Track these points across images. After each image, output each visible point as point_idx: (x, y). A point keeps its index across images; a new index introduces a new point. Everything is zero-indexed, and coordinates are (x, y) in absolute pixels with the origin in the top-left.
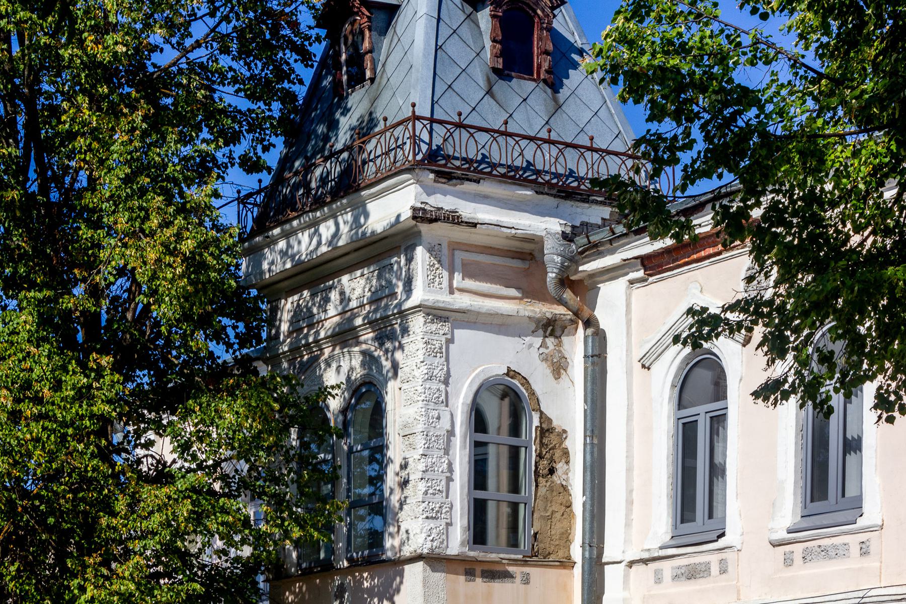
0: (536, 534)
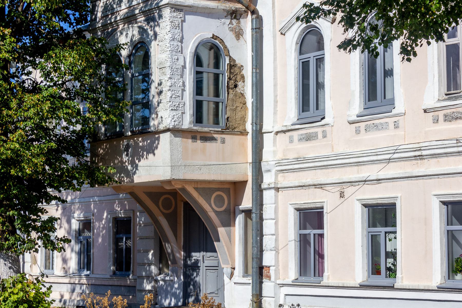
0: (228, 118)
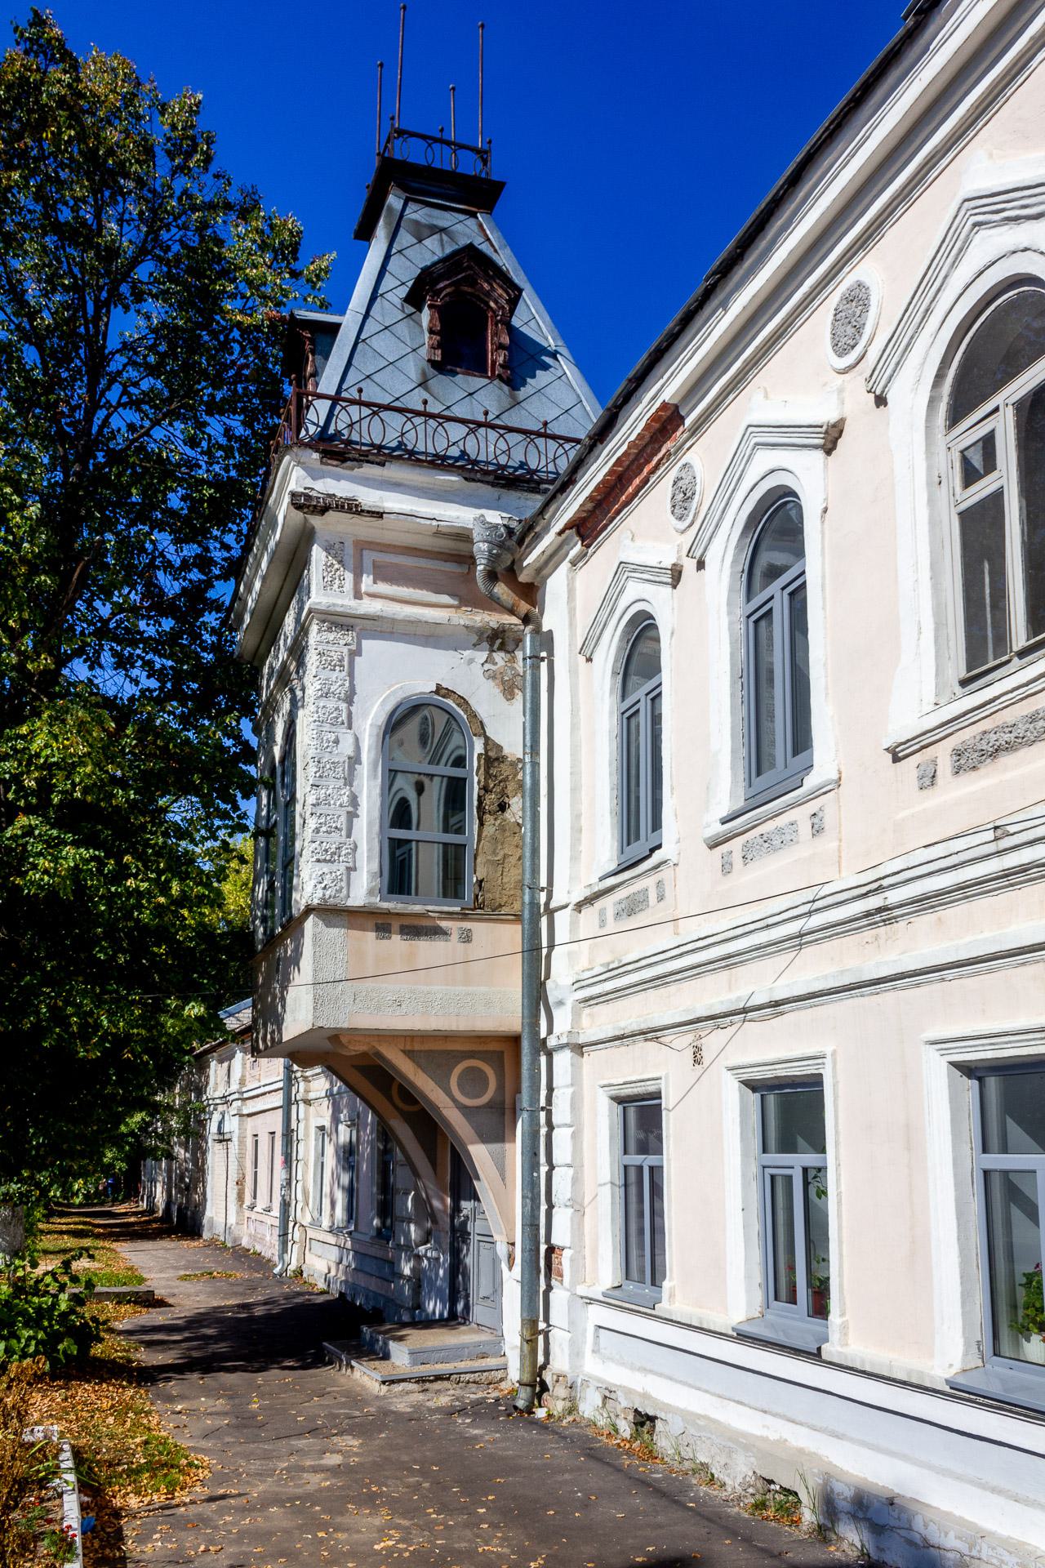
0: (480, 882)
